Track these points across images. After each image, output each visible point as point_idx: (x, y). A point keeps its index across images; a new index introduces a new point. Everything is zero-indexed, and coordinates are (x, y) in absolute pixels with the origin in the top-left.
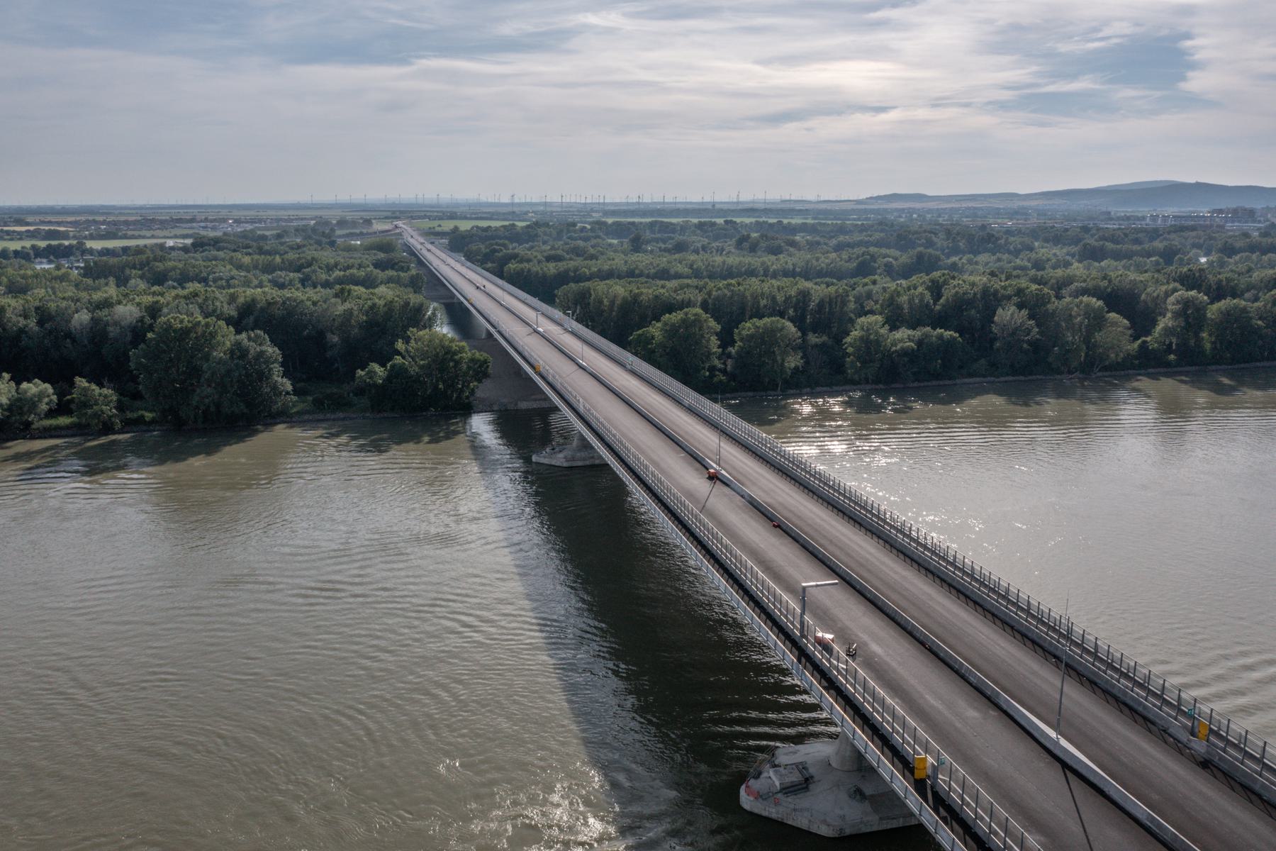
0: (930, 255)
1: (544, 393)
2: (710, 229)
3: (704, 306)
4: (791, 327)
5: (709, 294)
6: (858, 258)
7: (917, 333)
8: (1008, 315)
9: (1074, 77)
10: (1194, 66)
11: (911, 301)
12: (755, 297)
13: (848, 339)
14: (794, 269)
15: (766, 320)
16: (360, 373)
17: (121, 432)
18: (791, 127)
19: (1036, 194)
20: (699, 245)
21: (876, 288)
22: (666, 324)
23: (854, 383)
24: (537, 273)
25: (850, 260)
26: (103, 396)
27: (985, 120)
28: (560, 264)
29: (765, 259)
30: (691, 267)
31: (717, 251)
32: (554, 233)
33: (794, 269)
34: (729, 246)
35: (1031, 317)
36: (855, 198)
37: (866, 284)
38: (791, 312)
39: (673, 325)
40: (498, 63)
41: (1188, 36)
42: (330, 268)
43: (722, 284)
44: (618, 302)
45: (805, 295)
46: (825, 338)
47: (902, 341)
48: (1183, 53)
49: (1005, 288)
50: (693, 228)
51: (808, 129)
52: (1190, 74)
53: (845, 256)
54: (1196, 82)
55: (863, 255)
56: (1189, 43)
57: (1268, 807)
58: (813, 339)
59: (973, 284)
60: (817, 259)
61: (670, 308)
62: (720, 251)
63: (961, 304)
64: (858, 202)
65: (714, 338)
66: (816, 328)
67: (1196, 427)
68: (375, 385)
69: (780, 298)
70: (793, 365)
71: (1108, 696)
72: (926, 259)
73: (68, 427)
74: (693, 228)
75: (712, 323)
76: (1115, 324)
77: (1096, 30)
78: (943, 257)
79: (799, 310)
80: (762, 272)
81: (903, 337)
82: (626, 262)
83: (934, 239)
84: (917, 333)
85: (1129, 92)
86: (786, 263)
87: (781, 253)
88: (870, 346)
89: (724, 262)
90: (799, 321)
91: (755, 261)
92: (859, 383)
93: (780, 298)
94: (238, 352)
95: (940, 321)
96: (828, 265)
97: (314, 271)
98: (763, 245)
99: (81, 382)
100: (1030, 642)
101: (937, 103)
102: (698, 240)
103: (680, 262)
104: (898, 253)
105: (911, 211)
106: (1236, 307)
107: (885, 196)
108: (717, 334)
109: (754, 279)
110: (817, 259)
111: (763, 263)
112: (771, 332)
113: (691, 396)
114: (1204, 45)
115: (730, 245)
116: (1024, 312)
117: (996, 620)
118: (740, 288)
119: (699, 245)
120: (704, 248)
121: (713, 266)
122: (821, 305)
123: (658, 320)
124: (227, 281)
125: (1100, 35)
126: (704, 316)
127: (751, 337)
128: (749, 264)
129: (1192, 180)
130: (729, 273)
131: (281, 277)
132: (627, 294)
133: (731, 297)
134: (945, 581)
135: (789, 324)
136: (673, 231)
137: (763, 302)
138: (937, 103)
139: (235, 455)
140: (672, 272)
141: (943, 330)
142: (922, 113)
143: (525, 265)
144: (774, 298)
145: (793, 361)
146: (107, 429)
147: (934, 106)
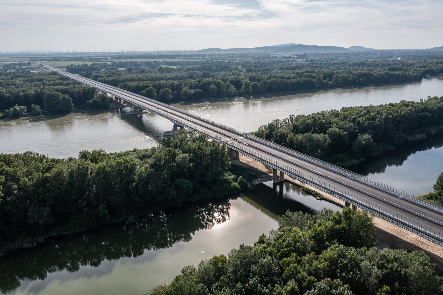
0: (207, 72)
1: (139, 94)
2: (150, 64)
3: (153, 86)
4: (170, 90)
5: (154, 84)
6: (189, 73)
7: (195, 90)
8: (212, 86)
11: (194, 84)
12: (163, 84)
13: (182, 92)
14: (173, 77)
15: (165, 89)
16: (87, 102)
17: (42, 115)
19: (254, 48)
20: (148, 71)
21: (188, 82)
22: (146, 90)
23: (183, 100)
24: (107, 80)
25: (187, 74)
26: (37, 108)
28: (112, 78)
29: (166, 75)
30: (147, 77)
31: (153, 72)
32: (100, 67)
33: (173, 77)
34: (156, 71)
35: (216, 87)
36: (198, 50)
37: (187, 81)
38: (170, 87)
39: (147, 90)
42: (49, 81)
43: (156, 82)
44: (135, 87)
45: (173, 84)
46: (177, 92)
47: (191, 92)
49: (212, 81)
50: (144, 64)
53: (186, 73)
55: (191, 73)
58: (175, 92)
59: (207, 80)
60: (179, 74)
61: (146, 87)
62: (154, 72)
63: (204, 84)
64: (198, 51)
65: (155, 93)
66: (175, 91)
67: (251, 107)
68: (91, 104)
69: (168, 84)
70: (171, 97)
72: (206, 73)
73: (28, 115)
74: (144, 64)
75: (155, 90)
76: (232, 87)
78: (210, 73)
79: (172, 87)
80: (165, 78)
81: (192, 91)
82: (130, 76)
83: (212, 67)
84: (195, 90)
86: (171, 76)
87: (170, 72)
88: (185, 92)
89: (155, 76)
90: (172, 89)
91: (163, 75)
92: (184, 100)
93: (168, 84)
94: (64, 98)
95: (200, 88)
96: (182, 76)
97: (45, 82)
98: (165, 70)
99: (33, 105)
102: (147, 69)
103: (144, 76)
104: (200, 72)
105: (216, 55)
106: (255, 83)
107: (207, 49)
108: (156, 92)
109: (163, 81)
110: (179, 74)
111: (166, 76)
112: (166, 91)
115: (156, 71)
116: (215, 86)
118: (420, 107)
119: (148, 71)
120: (149, 71)
121: (153, 77)
122: (176, 85)
123: (144, 90)
124: (22, 85)
126: (153, 88)
127: (163, 92)
128: (162, 76)
130: (157, 79)
131: (36, 83)
132: (137, 85)
133: (158, 85)
135: (170, 89)
136: (138, 65)
137: (165, 86)
139: (66, 117)
140: (142, 79)
143: (104, 78)
144: (167, 85)
145: (171, 97)
146: (39, 114)
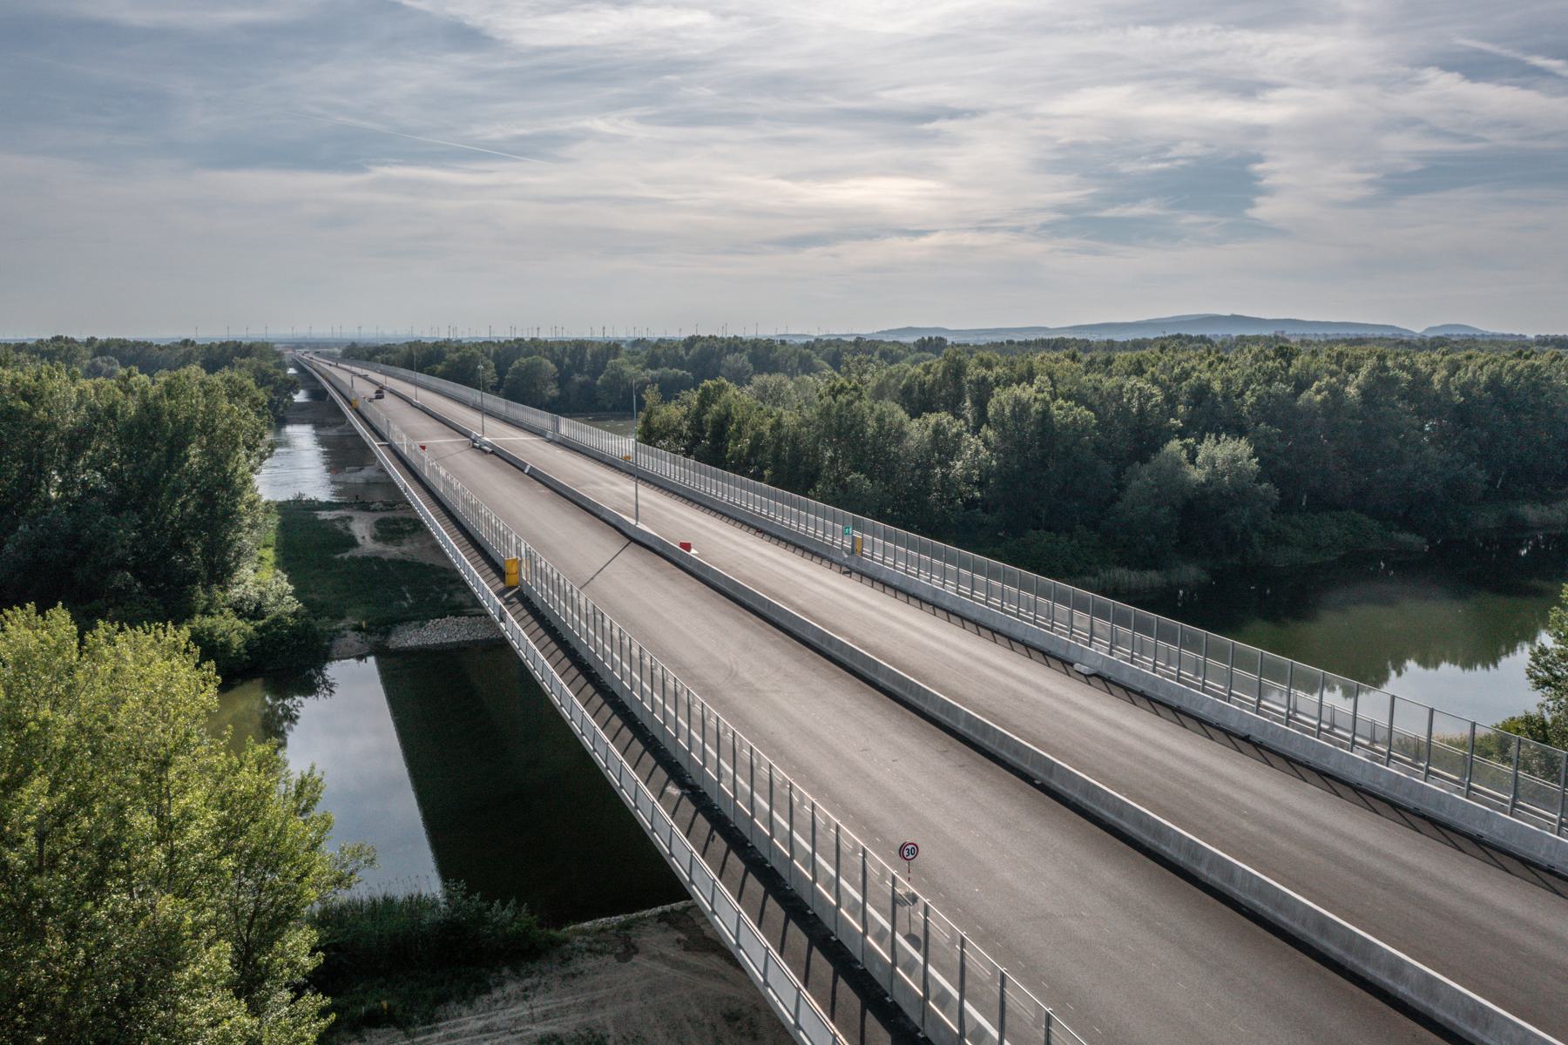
9: (1135, 200)
10: (1263, 192)
18: (813, 253)
27: (1035, 248)
40: (478, 172)
41: (1259, 159)
48: (1256, 177)
51: (833, 255)
52: (1259, 200)
54: (1265, 210)
56: (1258, 167)
57: (1235, 740)
71: (1181, 716)
77: (1165, 149)
85: (1193, 219)
100: (1222, 734)
101: (982, 227)
113: (543, 419)
114: (1278, 169)
117: (966, 623)
125: (1169, 155)
129: (1227, 313)
134: (999, 633)
138: (982, 227)
141: (765, 376)
142: (969, 239)
147: (980, 229)
